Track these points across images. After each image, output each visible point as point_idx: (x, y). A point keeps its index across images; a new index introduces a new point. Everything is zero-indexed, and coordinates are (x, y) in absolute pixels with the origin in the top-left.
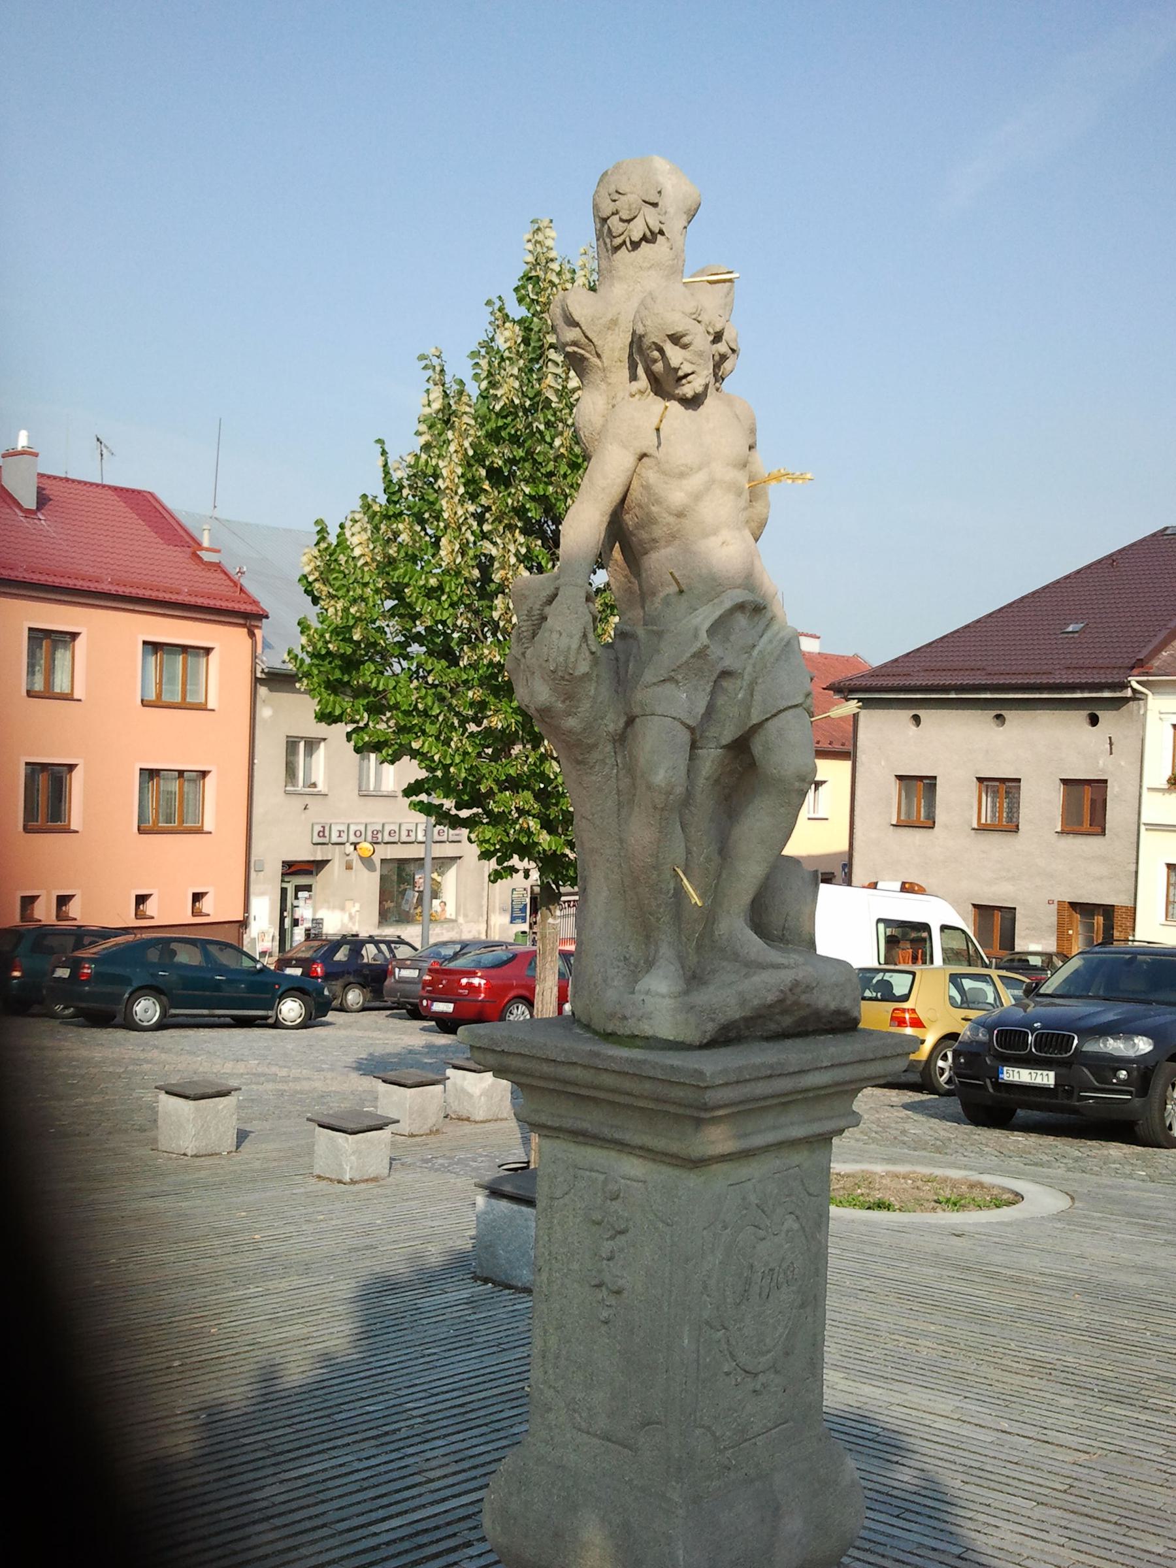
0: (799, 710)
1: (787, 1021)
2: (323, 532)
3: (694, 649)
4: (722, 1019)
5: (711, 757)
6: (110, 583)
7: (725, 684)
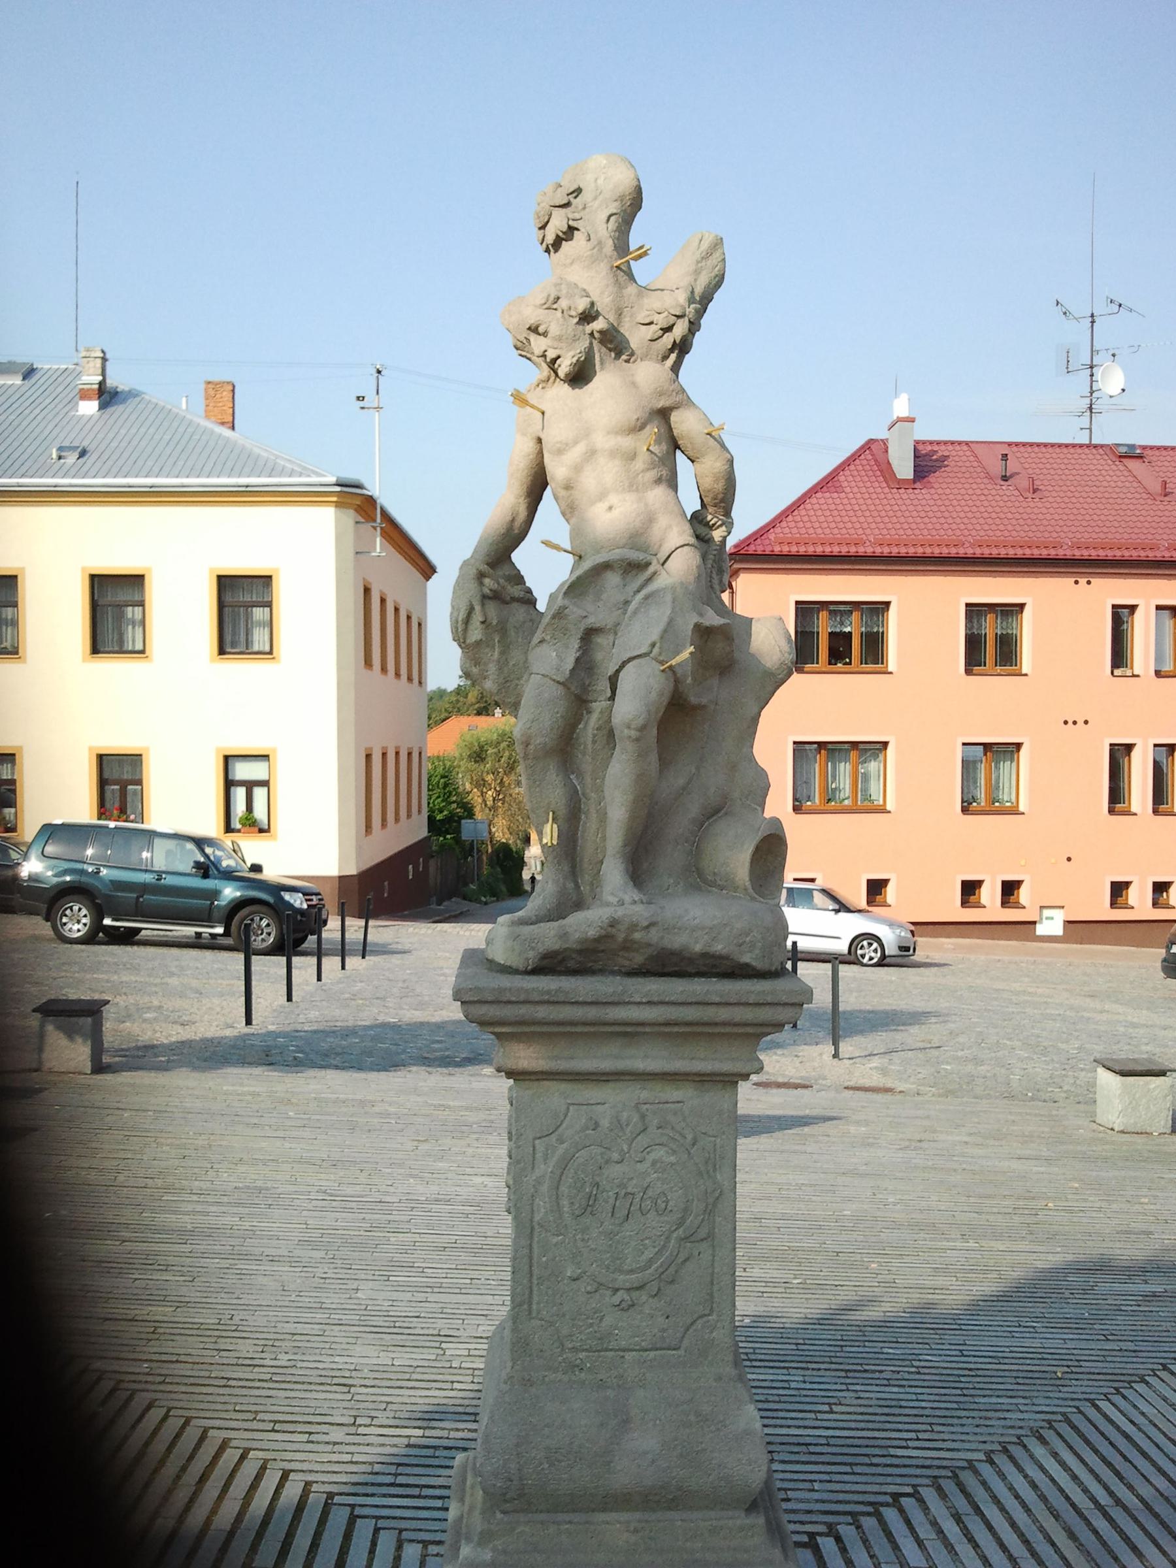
1: (638, 959)
4: (541, 949)
6: (1168, 549)
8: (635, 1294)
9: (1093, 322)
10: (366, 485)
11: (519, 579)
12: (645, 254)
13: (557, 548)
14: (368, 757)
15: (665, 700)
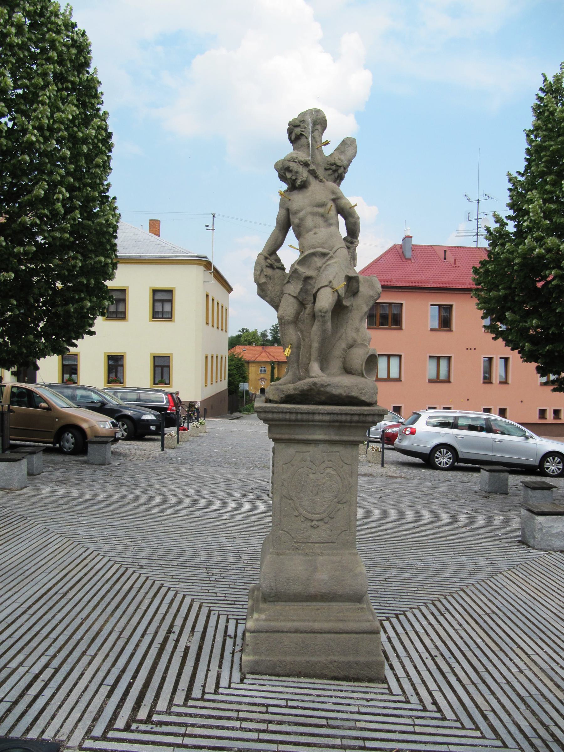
1: (323, 398)
8: (319, 522)
9: (478, 202)
10: (208, 257)
11: (279, 260)
12: (328, 143)
13: (294, 248)
14: (206, 357)
15: (334, 303)
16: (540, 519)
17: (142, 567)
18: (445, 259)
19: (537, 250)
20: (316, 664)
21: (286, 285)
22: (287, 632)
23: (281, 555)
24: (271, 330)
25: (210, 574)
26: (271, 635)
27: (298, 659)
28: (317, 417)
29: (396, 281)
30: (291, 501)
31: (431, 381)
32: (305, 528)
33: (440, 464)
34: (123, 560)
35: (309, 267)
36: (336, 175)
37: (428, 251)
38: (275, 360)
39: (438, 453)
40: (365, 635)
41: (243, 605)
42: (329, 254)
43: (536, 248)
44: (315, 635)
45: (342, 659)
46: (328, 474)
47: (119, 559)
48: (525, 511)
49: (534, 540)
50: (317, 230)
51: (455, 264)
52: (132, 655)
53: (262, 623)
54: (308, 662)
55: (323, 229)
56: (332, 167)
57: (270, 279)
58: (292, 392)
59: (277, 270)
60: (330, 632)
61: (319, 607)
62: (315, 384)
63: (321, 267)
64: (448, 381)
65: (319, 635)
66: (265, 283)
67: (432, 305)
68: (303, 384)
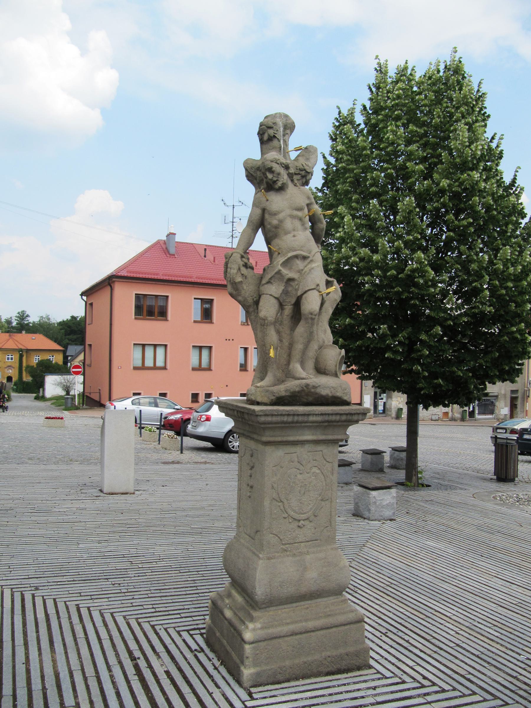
0: (315, 290)
1: (311, 399)
2: (376, 69)
3: (275, 271)
5: (288, 310)
7: (291, 283)
9: (233, 208)
16: (374, 493)
17: (37, 589)
18: (205, 256)
19: (352, 259)
20: (313, 663)
21: (266, 286)
22: (284, 636)
23: (272, 558)
24: (16, 317)
25: (116, 585)
26: (269, 642)
27: (297, 661)
28: (311, 418)
29: (163, 275)
30: (280, 504)
31: (194, 369)
32: (292, 529)
33: (233, 447)
34: (13, 582)
35: (290, 269)
36: (304, 180)
37: (189, 248)
38: (23, 348)
39: (231, 437)
40: (352, 626)
41: (179, 614)
42: (309, 257)
43: (351, 257)
44: (309, 634)
45: (334, 653)
46: (313, 473)
47: (9, 582)
48: (359, 487)
49: (370, 513)
50: (296, 233)
51: (214, 261)
52: (118, 694)
53: (260, 632)
54: (305, 663)
55: (300, 233)
56: (301, 172)
57: (246, 278)
58: (283, 394)
59: (249, 270)
60: (322, 629)
61: (306, 606)
62: (307, 385)
63: (302, 270)
64: (209, 369)
65: (312, 634)
66: (241, 281)
67: (195, 299)
68: (292, 385)
